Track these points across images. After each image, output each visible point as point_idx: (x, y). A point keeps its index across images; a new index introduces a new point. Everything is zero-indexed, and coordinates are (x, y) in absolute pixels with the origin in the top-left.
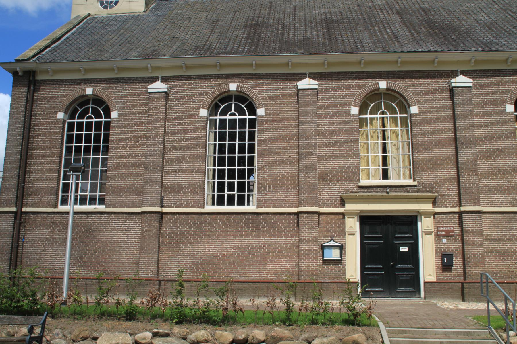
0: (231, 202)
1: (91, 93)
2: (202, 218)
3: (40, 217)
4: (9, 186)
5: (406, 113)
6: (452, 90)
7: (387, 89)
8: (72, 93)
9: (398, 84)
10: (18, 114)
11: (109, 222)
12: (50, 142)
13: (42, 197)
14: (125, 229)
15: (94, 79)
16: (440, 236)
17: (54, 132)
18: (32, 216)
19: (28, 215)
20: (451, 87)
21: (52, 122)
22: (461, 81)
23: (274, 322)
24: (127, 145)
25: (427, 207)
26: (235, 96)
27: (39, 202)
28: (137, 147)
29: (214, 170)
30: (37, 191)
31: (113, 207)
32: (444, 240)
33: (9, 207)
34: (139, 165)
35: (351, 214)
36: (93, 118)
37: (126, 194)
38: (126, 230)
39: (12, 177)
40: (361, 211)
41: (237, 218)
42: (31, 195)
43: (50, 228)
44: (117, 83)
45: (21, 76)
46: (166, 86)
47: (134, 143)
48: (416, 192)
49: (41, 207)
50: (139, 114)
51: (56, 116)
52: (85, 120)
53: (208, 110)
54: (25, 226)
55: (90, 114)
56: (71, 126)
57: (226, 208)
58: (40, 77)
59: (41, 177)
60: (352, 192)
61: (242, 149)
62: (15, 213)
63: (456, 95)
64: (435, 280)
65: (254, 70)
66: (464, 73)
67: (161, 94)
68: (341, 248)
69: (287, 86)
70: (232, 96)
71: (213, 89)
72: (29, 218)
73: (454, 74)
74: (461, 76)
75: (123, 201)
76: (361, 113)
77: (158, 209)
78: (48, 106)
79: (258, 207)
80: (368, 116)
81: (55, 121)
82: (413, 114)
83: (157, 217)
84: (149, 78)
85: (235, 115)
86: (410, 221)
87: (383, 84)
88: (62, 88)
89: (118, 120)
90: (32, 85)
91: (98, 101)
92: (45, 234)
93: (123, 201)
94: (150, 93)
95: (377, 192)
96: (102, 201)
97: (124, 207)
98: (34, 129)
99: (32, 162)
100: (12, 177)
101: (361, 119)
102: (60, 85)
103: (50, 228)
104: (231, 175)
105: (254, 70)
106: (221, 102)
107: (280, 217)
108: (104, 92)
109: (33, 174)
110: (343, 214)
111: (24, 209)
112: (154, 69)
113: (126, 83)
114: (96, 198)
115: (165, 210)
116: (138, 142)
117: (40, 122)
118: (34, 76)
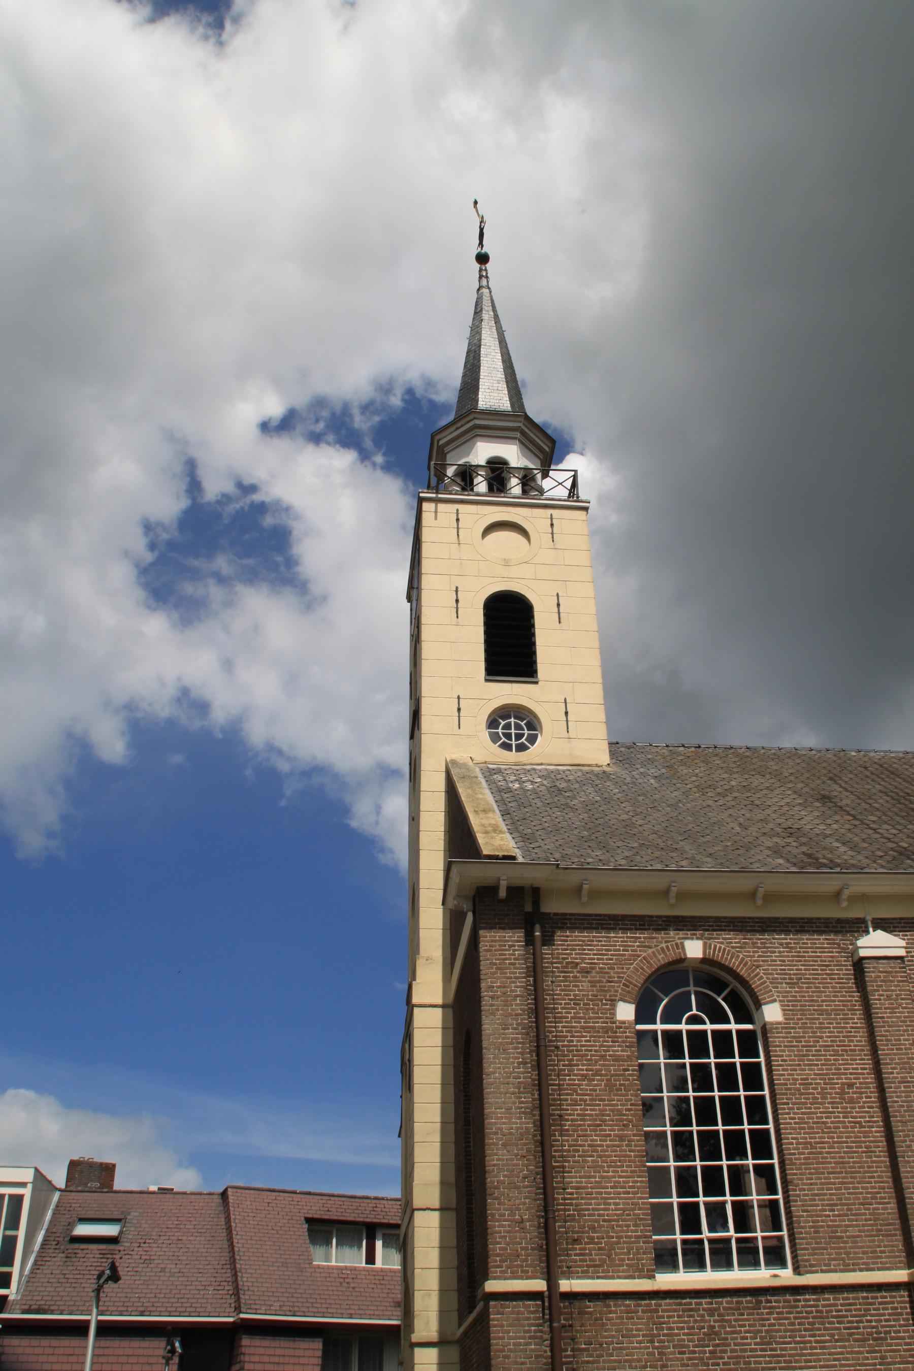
0: (722, 1258)
1: (699, 955)
3: (616, 1310)
4: (512, 1214)
5: (750, 1021)
6: (859, 965)
7: (704, 960)
8: (645, 952)
9: (731, 948)
10: (506, 1004)
11: (820, 1316)
12: (609, 1084)
13: (612, 1246)
14: (871, 1334)
15: (701, 918)
17: (617, 1059)
18: (591, 1307)
19: (577, 1303)
20: (856, 959)
21: (606, 1030)
22: (877, 943)
24: (824, 1095)
26: (695, 971)
27: (604, 1261)
28: (851, 1101)
30: (593, 1228)
31: (822, 1271)
33: (521, 1278)
34: (869, 1151)
36: (705, 1023)
37: (852, 1232)
38: (875, 1339)
39: (517, 1187)
42: (576, 1241)
43: (652, 1341)
44: (763, 931)
45: (501, 901)
46: (903, 943)
47: (842, 1089)
49: (612, 1278)
50: (837, 1011)
51: (614, 1014)
52: (683, 1027)
54: (573, 1339)
55: (694, 1011)
58: (551, 906)
59: (598, 1185)
62: (241, 1312)
63: (870, 976)
65: (672, 906)
66: (886, 925)
70: (687, 971)
72: (582, 1313)
73: (859, 927)
74: (879, 932)
75: (848, 1253)
76: (639, 1019)
78: (585, 985)
80: (659, 1027)
81: (613, 1028)
82: (772, 1023)
84: (839, 921)
87: (694, 949)
88: (618, 937)
89: (785, 1026)
90: (537, 927)
92: (639, 1360)
93: (848, 1253)
96: (775, 1257)
97: (854, 1270)
98: (557, 1047)
99: (562, 1143)
100: (517, 1187)
101: (641, 1034)
102: (609, 929)
103: (652, 1341)
104: (713, 1184)
105: (672, 906)
106: (665, 985)
109: (574, 1179)
111: (565, 1285)
112: (863, 898)
113: (787, 932)
116: (851, 1085)
117: (569, 1027)
118: (536, 903)
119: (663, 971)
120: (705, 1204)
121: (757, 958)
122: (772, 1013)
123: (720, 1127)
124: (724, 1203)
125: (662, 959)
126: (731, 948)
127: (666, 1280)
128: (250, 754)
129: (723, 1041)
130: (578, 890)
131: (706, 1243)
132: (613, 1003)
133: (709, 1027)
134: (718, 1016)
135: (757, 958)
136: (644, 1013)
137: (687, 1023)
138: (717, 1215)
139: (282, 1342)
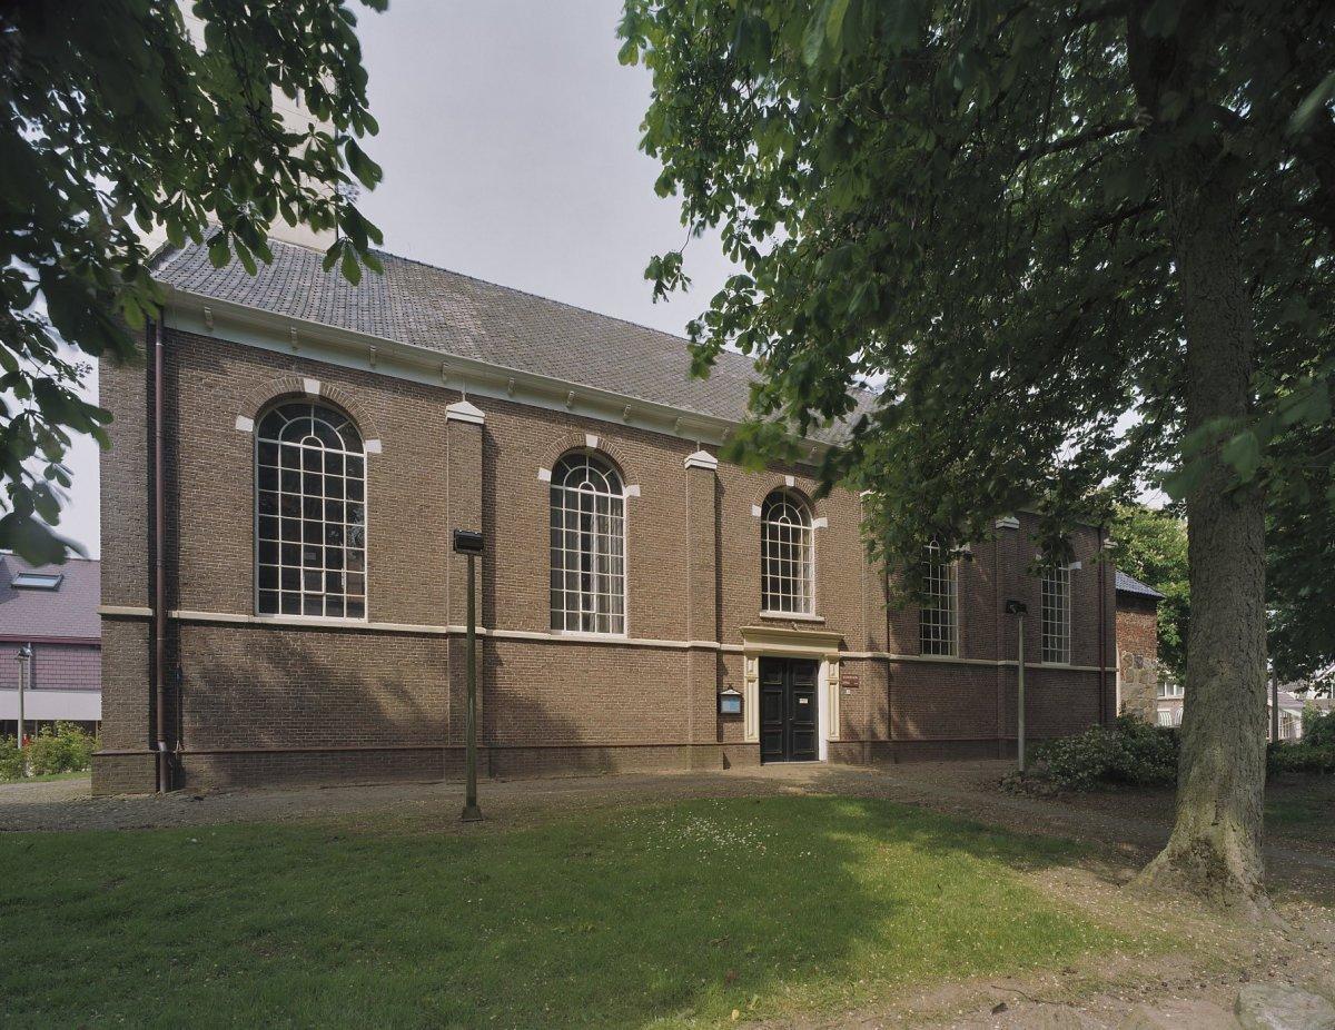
0: (313, 606)
2: (550, 649)
7: (597, 450)
8: (279, 382)
16: (844, 686)
17: (234, 459)
23: (1306, 766)
25: (834, 651)
29: (795, 593)
32: (848, 692)
35: (750, 655)
40: (765, 651)
41: (603, 651)
48: (826, 630)
52: (579, 490)
53: (256, 423)
55: (587, 482)
56: (267, 454)
57: (932, 657)
60: (751, 624)
61: (335, 511)
62: (150, 620)
64: (838, 739)
66: (704, 447)
67: (472, 427)
68: (740, 698)
69: (420, 406)
71: (559, 439)
77: (715, 645)
79: (632, 636)
81: (233, 436)
83: (713, 656)
85: (591, 489)
86: (810, 666)
87: (790, 481)
91: (329, 410)
94: (450, 419)
95: (773, 626)
107: (665, 653)
108: (618, 448)
110: (740, 653)
111: (497, 633)
114: (348, 608)
115: (725, 647)
119: (574, 452)
120: (305, 571)
121: (367, 405)
122: (372, 446)
123: (780, 577)
124: (321, 572)
125: (282, 389)
126: (341, 392)
127: (566, 634)
128: (306, 220)
129: (602, 502)
130: (673, 422)
131: (324, 599)
132: (234, 415)
133: (790, 525)
134: (795, 521)
135: (367, 405)
136: (557, 478)
137: (304, 443)
138: (936, 632)
139: (54, 653)
